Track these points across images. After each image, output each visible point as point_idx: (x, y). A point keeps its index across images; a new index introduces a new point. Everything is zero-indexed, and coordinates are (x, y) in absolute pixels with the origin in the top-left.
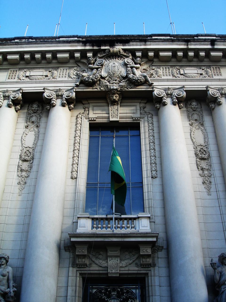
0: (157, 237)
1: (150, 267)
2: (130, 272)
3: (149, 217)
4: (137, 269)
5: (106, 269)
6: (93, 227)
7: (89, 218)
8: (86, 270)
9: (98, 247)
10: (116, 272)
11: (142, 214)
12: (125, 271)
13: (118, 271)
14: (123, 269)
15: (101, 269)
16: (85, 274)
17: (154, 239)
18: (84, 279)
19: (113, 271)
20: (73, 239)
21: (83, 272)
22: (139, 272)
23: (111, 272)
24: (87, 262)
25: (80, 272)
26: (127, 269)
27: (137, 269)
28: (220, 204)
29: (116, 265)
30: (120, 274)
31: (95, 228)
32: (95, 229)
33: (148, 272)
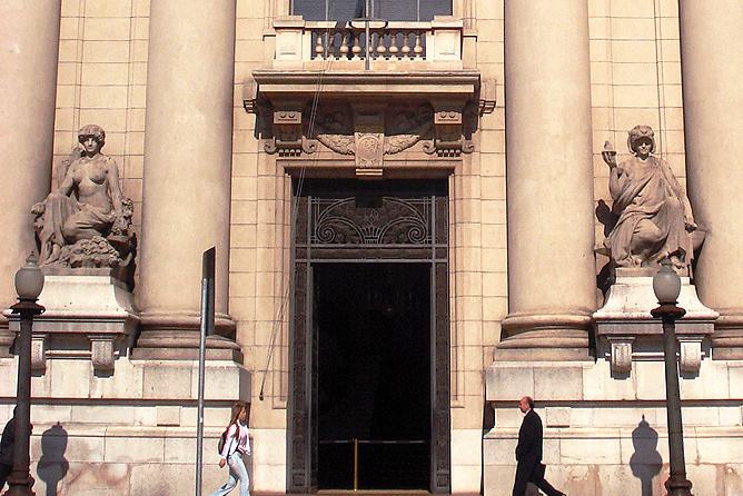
0: (477, 84)
1: (458, 155)
2: (409, 164)
3: (460, 29)
4: (427, 157)
5: (352, 157)
6: (314, 54)
7: (304, 29)
8: (304, 161)
9: (335, 111)
10: (376, 165)
11: (443, 21)
12: (398, 161)
13: (381, 164)
14: (388, 157)
15: (337, 156)
16: (299, 169)
17: (470, 89)
18: (295, 182)
19: (369, 164)
20: (264, 88)
21: (293, 164)
22: (431, 164)
23: (362, 165)
24: (305, 141)
25: (286, 164)
26: (400, 156)
27: (427, 157)
28: (80, 49)
29: (369, 151)
30: (385, 170)
31: (319, 55)
32: (319, 58)
33: (453, 164)
